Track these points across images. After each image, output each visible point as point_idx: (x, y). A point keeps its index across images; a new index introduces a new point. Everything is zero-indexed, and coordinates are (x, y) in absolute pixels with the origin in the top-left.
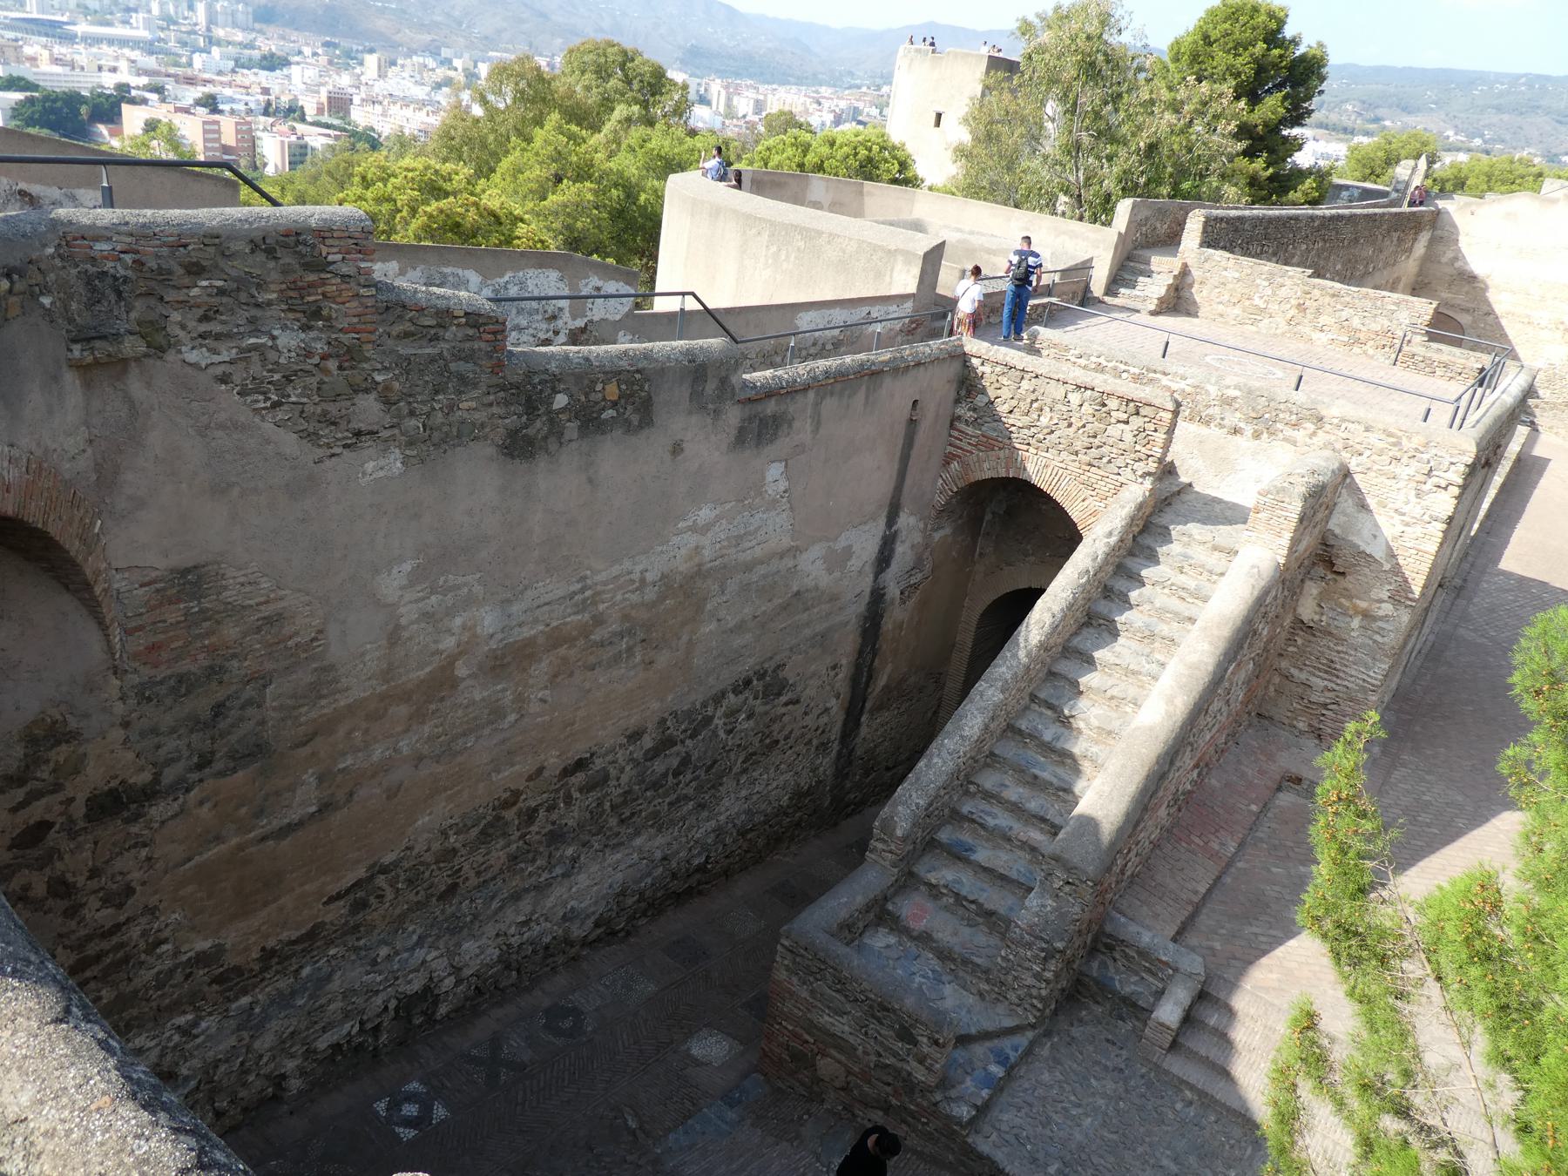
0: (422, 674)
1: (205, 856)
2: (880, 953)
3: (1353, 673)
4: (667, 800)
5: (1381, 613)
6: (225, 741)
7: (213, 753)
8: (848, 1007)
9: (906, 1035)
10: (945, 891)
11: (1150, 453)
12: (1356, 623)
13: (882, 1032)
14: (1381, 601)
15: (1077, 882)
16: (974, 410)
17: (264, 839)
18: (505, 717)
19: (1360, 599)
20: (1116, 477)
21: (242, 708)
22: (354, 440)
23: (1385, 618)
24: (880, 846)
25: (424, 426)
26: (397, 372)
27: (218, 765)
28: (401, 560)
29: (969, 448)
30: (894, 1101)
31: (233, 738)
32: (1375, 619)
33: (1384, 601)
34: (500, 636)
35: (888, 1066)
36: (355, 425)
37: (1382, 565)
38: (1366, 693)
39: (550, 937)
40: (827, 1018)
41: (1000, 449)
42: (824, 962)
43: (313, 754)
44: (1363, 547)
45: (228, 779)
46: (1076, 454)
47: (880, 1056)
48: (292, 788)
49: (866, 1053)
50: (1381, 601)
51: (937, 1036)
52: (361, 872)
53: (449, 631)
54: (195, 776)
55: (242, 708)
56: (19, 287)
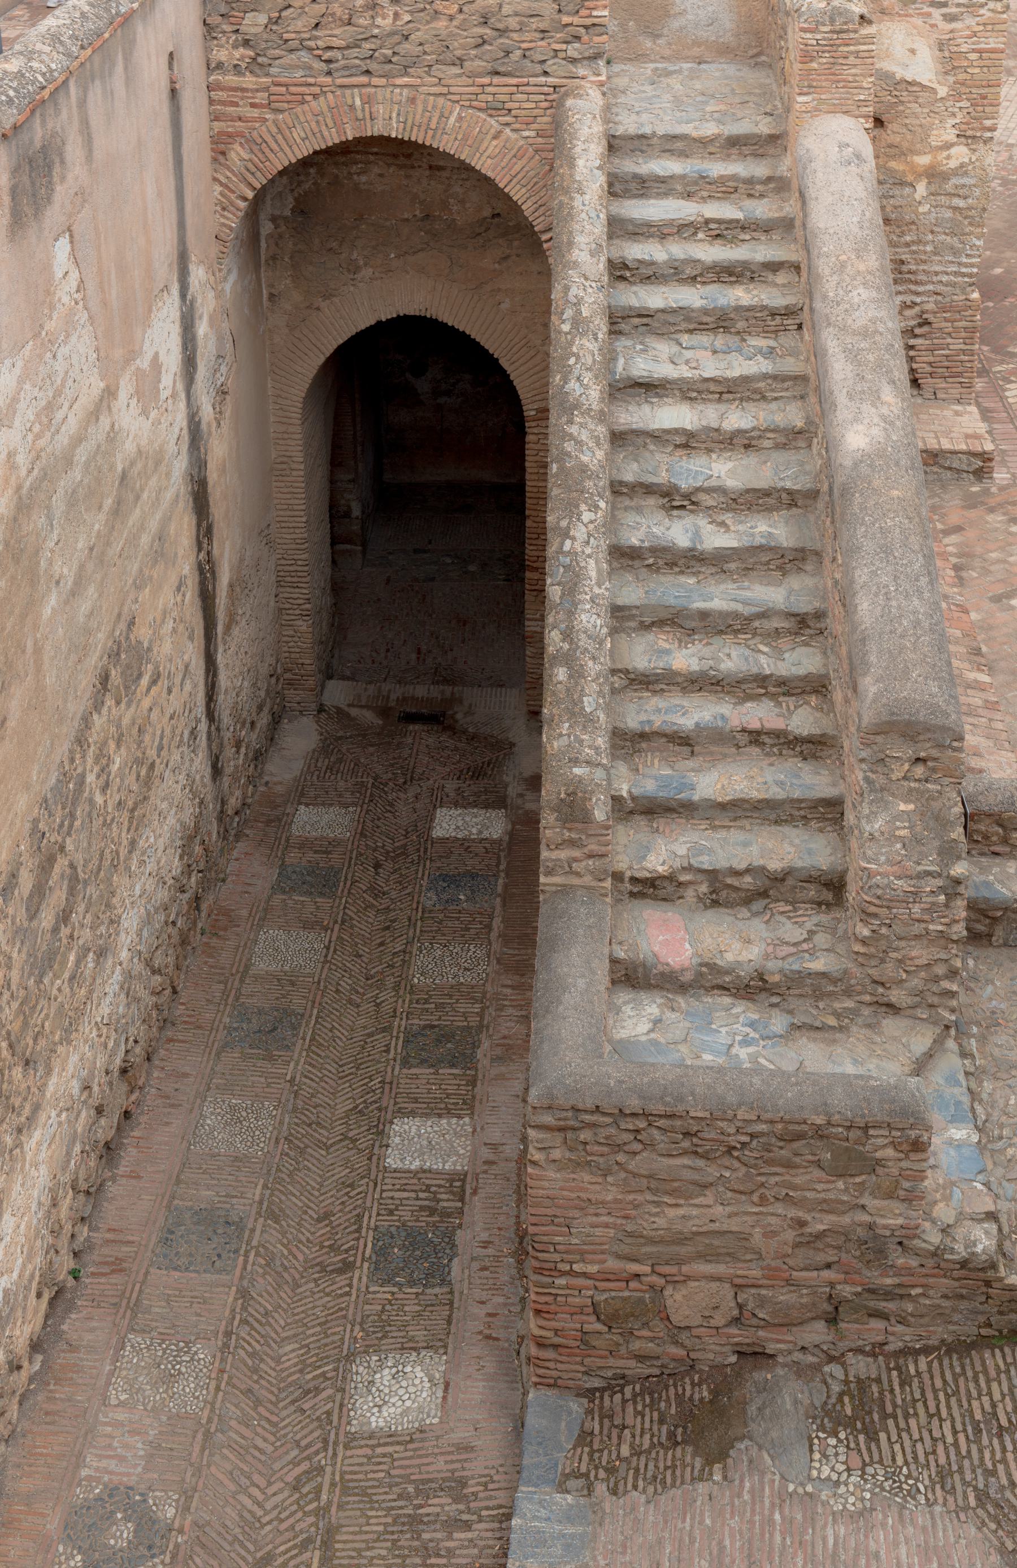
2: (654, 1043)
3: (938, 268)
5: (953, 164)
8: (713, 1172)
10: (684, 878)
11: (588, 22)
12: (921, 189)
13: (797, 1181)
14: (948, 146)
15: (934, 753)
16: (246, 43)
19: (919, 153)
20: (542, 79)
23: (961, 170)
29: (255, 113)
30: (846, 1291)
32: (945, 177)
33: (952, 145)
35: (820, 1236)
37: (934, 91)
38: (963, 291)
40: (672, 1212)
41: (315, 96)
42: (646, 1115)
44: (900, 73)
46: (460, 61)
47: (802, 1224)
50: (948, 146)
51: (913, 1134)
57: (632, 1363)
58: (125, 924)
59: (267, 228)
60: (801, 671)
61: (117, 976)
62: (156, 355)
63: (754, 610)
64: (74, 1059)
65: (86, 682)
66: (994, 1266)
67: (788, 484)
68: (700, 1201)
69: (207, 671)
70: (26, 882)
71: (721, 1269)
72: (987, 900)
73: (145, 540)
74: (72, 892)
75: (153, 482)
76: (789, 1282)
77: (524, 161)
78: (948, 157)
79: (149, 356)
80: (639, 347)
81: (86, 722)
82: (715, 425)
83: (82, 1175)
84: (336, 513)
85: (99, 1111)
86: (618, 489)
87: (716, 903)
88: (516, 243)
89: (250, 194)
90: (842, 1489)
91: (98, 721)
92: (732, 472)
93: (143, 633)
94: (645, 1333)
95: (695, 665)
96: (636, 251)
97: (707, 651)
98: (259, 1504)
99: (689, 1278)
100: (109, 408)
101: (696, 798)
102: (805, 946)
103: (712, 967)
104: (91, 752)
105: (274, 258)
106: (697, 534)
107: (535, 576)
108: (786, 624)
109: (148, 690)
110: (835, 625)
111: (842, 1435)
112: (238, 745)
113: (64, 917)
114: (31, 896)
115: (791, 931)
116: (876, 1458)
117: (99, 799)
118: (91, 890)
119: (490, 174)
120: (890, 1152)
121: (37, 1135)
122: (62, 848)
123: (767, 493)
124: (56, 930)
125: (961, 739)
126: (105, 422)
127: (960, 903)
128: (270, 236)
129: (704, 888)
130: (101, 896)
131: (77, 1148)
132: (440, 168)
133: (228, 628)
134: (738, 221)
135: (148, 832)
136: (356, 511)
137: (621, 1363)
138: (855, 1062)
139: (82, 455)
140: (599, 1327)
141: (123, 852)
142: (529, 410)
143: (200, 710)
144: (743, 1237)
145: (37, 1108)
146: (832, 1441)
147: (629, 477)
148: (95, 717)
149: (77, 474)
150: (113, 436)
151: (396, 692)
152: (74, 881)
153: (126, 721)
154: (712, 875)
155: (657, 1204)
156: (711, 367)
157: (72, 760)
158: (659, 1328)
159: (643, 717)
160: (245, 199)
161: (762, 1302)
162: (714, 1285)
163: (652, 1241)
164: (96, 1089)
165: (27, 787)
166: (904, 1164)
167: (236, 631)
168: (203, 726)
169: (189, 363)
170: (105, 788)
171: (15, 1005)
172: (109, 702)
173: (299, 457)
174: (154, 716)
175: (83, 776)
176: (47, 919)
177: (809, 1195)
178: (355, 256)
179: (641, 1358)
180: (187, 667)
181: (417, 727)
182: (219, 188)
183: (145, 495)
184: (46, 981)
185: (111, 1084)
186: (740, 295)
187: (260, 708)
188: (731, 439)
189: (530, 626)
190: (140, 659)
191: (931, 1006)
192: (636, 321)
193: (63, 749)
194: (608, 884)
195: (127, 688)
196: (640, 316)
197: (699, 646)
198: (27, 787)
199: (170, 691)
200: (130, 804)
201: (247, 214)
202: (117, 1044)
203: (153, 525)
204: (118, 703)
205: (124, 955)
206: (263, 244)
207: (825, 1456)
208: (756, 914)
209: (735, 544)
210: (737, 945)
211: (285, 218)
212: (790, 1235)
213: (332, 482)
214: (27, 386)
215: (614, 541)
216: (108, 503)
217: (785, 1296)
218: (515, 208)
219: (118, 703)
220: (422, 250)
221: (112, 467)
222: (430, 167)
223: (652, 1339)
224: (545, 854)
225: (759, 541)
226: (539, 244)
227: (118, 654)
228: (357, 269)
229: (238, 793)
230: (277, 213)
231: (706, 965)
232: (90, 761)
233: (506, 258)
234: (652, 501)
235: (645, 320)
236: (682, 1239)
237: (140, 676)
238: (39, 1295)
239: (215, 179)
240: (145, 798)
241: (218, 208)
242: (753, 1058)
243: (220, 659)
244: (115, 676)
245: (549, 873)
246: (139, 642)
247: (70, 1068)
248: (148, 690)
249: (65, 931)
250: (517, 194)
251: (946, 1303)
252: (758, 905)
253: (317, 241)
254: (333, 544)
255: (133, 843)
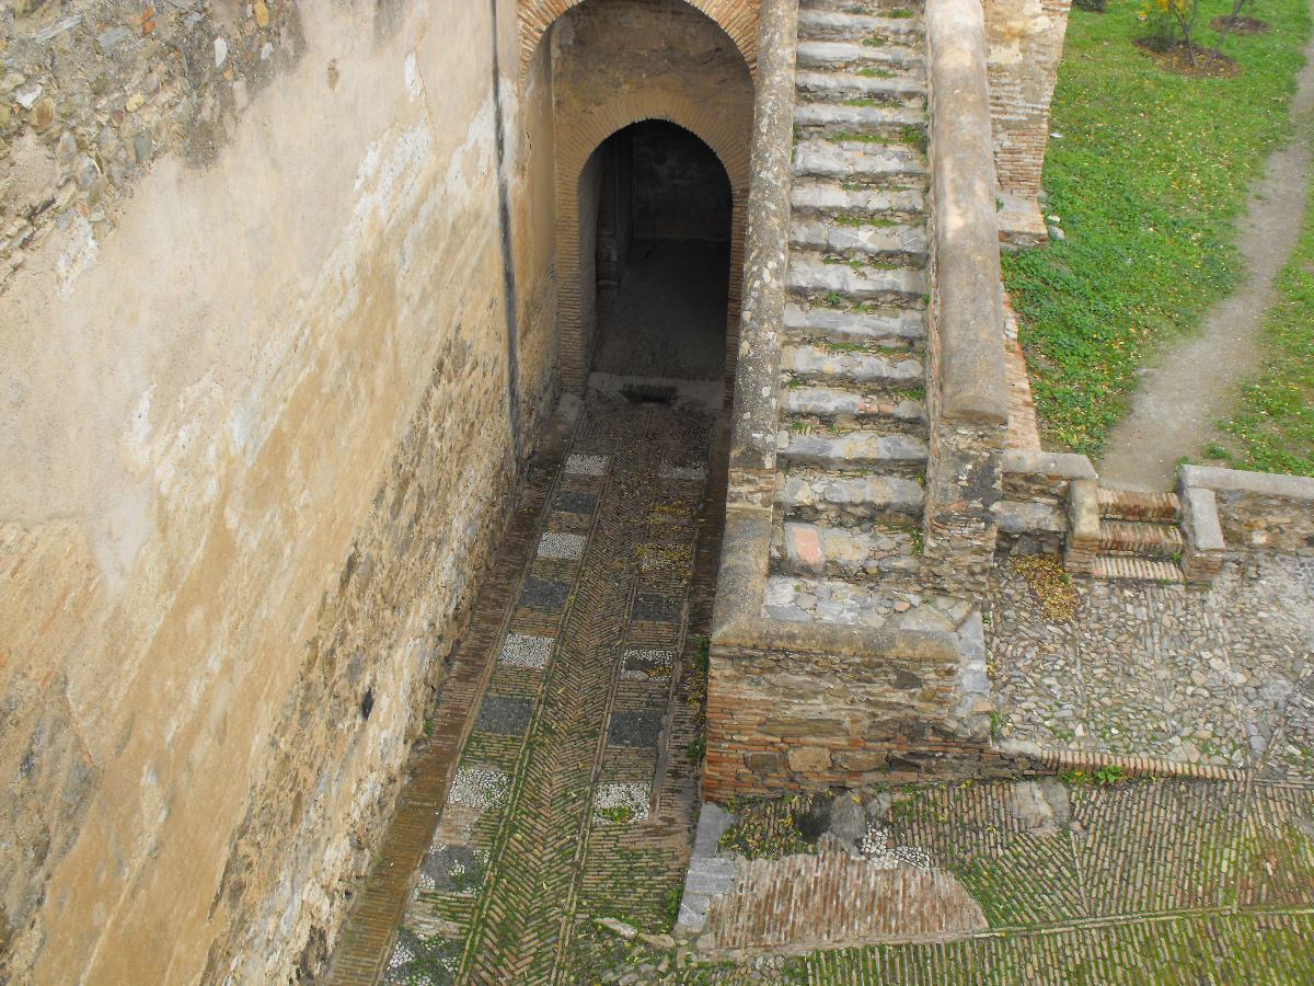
0: (200, 552)
1: (89, 968)
4: (417, 556)
5: (1038, 29)
6: (51, 802)
7: (46, 830)
9: (907, 680)
13: (875, 691)
14: (1035, 16)
17: (133, 894)
18: (282, 553)
21: (52, 741)
22: (30, 230)
24: (745, 489)
25: (99, 162)
26: (44, 81)
27: (57, 842)
28: (135, 397)
31: (57, 792)
33: (1039, 15)
34: (250, 446)
36: (22, 205)
39: (379, 787)
40: (796, 708)
43: (141, 743)
45: (75, 849)
48: (136, 808)
49: (855, 721)
50: (1035, 16)
52: (226, 852)
53: (208, 472)
54: (40, 875)
55: (52, 741)
56: (35, 122)
57: (766, 791)
58: (455, 524)
59: (555, 53)
60: (908, 376)
61: (451, 558)
62: (477, 142)
63: (880, 333)
64: (423, 607)
65: (428, 369)
66: (986, 741)
67: (908, 249)
68: (814, 701)
69: (510, 363)
70: (390, 496)
71: (823, 741)
72: (1010, 528)
73: (468, 272)
74: (420, 503)
75: (474, 232)
76: (864, 749)
77: (739, 10)
78: (1035, 24)
79: (471, 143)
80: (813, 148)
81: (428, 393)
82: (862, 205)
83: (430, 676)
84: (599, 258)
85: (440, 638)
86: (793, 246)
87: (841, 524)
88: (732, 70)
89: (544, 28)
90: (882, 858)
91: (437, 394)
92: (870, 240)
93: (466, 335)
94: (774, 775)
95: (838, 369)
96: (815, 79)
97: (847, 360)
98: (540, 859)
99: (803, 745)
100: (443, 179)
101: (832, 456)
102: (894, 552)
103: (834, 563)
104: (431, 413)
105: (561, 74)
106: (844, 281)
107: (735, 306)
108: (900, 344)
109: (470, 374)
110: (934, 344)
111: (886, 831)
112: (530, 412)
113: (417, 518)
114: (393, 505)
115: (886, 542)
116: (904, 841)
117: (437, 445)
118: (433, 503)
119: (715, 19)
120: (933, 676)
121: (400, 651)
122: (413, 475)
123: (891, 255)
124: (410, 527)
125: (1005, 423)
126: (440, 189)
127: (994, 528)
128: (558, 59)
129: (833, 514)
130: (439, 507)
131: (427, 660)
132: (680, 13)
133: (524, 335)
134: (887, 61)
135: (469, 467)
136: (614, 258)
137: (758, 790)
138: (918, 623)
139: (424, 211)
140: (746, 770)
141: (454, 480)
142: (736, 189)
143: (505, 389)
144: (838, 723)
145: (399, 636)
146: (879, 834)
147: (802, 239)
148: (434, 390)
149: (421, 224)
150: (445, 198)
151: (637, 382)
152: (421, 496)
153: (455, 394)
154: (841, 506)
155: (787, 703)
156: (864, 165)
157: (419, 418)
158: (783, 773)
159: (801, 402)
160: (541, 32)
161: (846, 759)
162: (819, 749)
163: (782, 724)
164: (437, 625)
165: (389, 434)
166: (941, 683)
167: (530, 336)
168: (507, 400)
169: (500, 144)
170: (441, 437)
171: (385, 572)
172: (444, 381)
173: (575, 217)
174: (474, 390)
175: (426, 429)
176: (404, 519)
177: (882, 699)
178: (617, 75)
179: (770, 788)
180: (496, 359)
181: (652, 405)
182: (521, 23)
183: (468, 240)
184: (404, 558)
185: (447, 623)
186: (885, 114)
187: (546, 389)
188: (872, 216)
189: (730, 340)
190: (464, 354)
191: (968, 590)
192: (812, 129)
193: (413, 409)
194: (771, 508)
195: (456, 372)
196: (815, 126)
197: (841, 356)
198: (389, 434)
199: (484, 374)
200: (458, 448)
201: (541, 42)
202: (451, 599)
203: (473, 261)
204: (450, 381)
205: (455, 545)
206: (553, 62)
207: (873, 841)
208: (864, 531)
209: (870, 288)
210: (850, 551)
211: (569, 46)
212: (867, 722)
213: (598, 236)
214: (386, 161)
215: (788, 282)
216: (442, 245)
217: (860, 756)
218: (731, 43)
219: (450, 381)
220: (665, 72)
221: (445, 221)
222: (673, 12)
223: (778, 778)
224: (731, 489)
225: (887, 287)
226: (747, 71)
227: (450, 349)
228: (619, 85)
229: (530, 445)
230: (563, 42)
231: (831, 562)
232: (431, 420)
233: (724, 81)
234: (817, 255)
235: (818, 129)
236: (799, 723)
237: (464, 364)
238: (405, 742)
239: (520, 16)
240: (468, 445)
241: (521, 38)
242: (853, 619)
243: (519, 355)
244: (447, 362)
245: (734, 500)
246: (464, 342)
247: (422, 613)
248: (470, 374)
249: (416, 528)
250: (734, 33)
251: (954, 761)
252: (866, 525)
253: (590, 63)
254: (597, 280)
255: (460, 474)
